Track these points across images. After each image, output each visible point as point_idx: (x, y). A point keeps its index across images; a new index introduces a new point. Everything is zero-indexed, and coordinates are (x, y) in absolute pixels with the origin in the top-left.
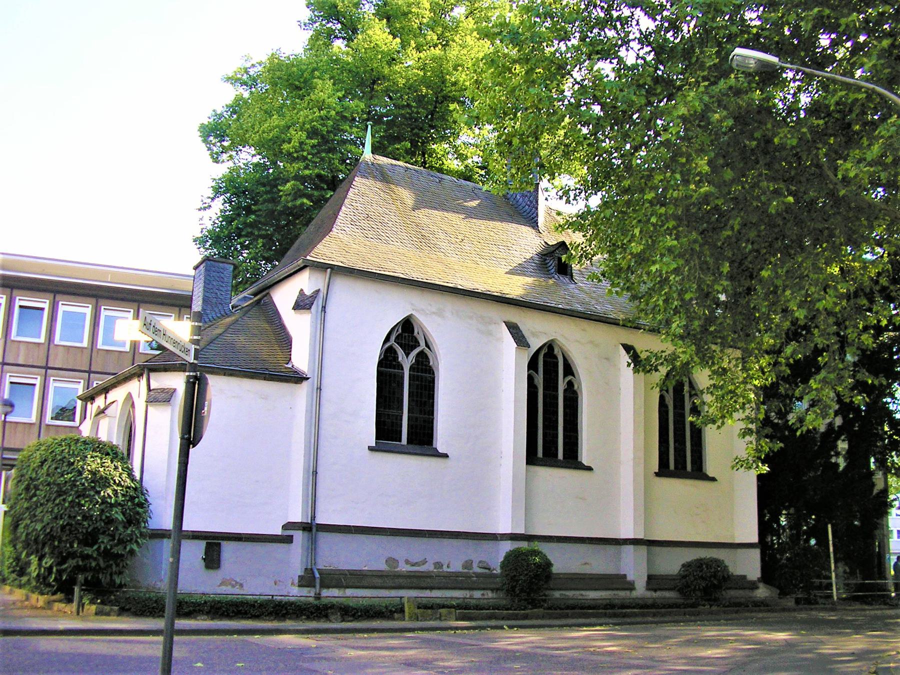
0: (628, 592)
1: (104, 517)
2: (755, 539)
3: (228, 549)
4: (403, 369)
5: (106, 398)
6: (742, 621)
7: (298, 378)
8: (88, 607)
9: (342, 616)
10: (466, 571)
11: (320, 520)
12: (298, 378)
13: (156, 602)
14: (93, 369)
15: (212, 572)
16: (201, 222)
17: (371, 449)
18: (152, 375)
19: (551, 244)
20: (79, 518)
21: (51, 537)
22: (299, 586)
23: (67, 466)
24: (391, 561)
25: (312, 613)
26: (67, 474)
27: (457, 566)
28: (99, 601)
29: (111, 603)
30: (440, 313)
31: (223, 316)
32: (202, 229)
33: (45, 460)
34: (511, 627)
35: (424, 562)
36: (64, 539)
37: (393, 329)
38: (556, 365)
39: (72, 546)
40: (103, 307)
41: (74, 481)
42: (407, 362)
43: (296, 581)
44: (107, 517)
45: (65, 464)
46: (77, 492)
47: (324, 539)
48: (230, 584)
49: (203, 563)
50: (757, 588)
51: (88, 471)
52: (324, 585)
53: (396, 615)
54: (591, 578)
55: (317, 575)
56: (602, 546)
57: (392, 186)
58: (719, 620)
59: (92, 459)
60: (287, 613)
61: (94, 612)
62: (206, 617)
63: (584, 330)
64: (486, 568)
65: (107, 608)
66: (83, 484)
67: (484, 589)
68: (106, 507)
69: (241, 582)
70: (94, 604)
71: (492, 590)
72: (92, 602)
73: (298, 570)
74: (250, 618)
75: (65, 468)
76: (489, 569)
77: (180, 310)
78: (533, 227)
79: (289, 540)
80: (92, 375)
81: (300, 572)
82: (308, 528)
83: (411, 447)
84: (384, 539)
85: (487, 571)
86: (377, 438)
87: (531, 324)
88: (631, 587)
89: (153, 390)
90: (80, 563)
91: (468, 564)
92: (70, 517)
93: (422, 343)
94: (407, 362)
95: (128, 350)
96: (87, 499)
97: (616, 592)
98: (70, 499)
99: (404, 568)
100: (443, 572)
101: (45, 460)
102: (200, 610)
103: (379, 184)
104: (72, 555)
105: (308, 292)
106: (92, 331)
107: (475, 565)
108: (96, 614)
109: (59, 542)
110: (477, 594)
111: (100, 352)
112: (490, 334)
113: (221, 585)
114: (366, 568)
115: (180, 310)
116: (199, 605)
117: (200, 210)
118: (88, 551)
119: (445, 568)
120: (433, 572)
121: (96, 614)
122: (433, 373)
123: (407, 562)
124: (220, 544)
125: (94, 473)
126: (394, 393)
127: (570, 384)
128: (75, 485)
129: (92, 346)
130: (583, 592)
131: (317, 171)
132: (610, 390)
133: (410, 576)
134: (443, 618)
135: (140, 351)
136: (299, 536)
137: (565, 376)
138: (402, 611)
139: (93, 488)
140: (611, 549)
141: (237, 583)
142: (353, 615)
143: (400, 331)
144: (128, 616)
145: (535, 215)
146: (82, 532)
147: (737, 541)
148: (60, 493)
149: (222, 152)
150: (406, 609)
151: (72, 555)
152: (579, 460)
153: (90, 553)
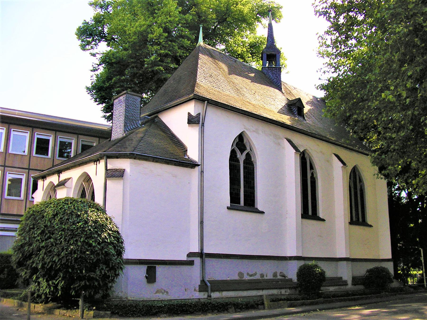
0: (344, 287)
1: (104, 252)
2: (390, 256)
3: (160, 270)
4: (239, 162)
5: (59, 177)
6: (405, 300)
7: (192, 165)
8: (87, 312)
9: (235, 309)
10: (274, 278)
11: (206, 251)
12: (192, 165)
13: (135, 307)
14: (6, 165)
15: (151, 285)
16: (91, 78)
17: (228, 208)
18: (108, 160)
19: (291, 99)
20: (88, 253)
21: (66, 266)
22: (199, 291)
23: (75, 217)
24: (241, 274)
25: (220, 308)
26: (78, 223)
27: (270, 276)
28: (94, 308)
29: (105, 309)
30: (256, 131)
31: (137, 128)
32: (92, 82)
33: (57, 214)
34: (321, 310)
35: (255, 274)
36: (76, 267)
37: (235, 139)
38: (306, 163)
39: (81, 272)
40: (12, 130)
41: (83, 227)
42: (242, 157)
43: (197, 289)
44: (106, 252)
45: (74, 216)
46: (86, 235)
47: (209, 262)
48: (161, 292)
49: (145, 280)
50: (393, 282)
51: (92, 221)
52: (213, 291)
53: (260, 306)
54: (331, 280)
55: (209, 284)
56: (330, 262)
57: (217, 61)
58: (396, 299)
59: (91, 213)
60: (209, 309)
61: (92, 316)
62: (165, 315)
63: (318, 145)
64: (283, 276)
65: (102, 313)
66: (90, 230)
67: (286, 288)
68: (105, 245)
69: (167, 290)
70: (91, 310)
71: (290, 288)
72: (90, 309)
73: (198, 282)
74: (189, 314)
75: (75, 219)
76: (285, 277)
77: (56, 133)
78: (279, 90)
79: (191, 263)
80: (6, 168)
81: (199, 283)
82: (201, 255)
83: (247, 208)
84: (235, 261)
85: (284, 278)
86: (231, 203)
87: (298, 139)
88: (345, 283)
89: (109, 170)
90: (88, 283)
91: (241, 274)
92: (81, 252)
93: (248, 148)
94: (242, 157)
95: (27, 154)
96: (93, 240)
97: (340, 287)
98: (82, 240)
99: (246, 278)
100: (265, 279)
101: (57, 214)
102: (162, 311)
103: (210, 59)
104: (81, 278)
105: (193, 114)
106: (6, 143)
107: (278, 275)
108: (94, 317)
109: (73, 270)
110: (283, 291)
111: (10, 155)
112: (279, 144)
113: (156, 293)
114: (229, 279)
115: (56, 133)
116: (161, 307)
117: (92, 71)
118: (92, 275)
119: (265, 278)
120: (260, 279)
121: (94, 317)
122: (253, 166)
123: (248, 274)
124: (155, 267)
125: (96, 222)
126: (236, 176)
127: (312, 174)
128: (84, 230)
129: (6, 151)
130: (328, 288)
131: (166, 51)
132: (330, 178)
133: (250, 282)
134: (282, 306)
135: (34, 155)
136: (197, 261)
137: (310, 170)
138: (263, 304)
139: (97, 232)
140: (334, 263)
141: (165, 291)
142: (240, 308)
143: (238, 140)
144: (116, 317)
145: (279, 84)
146: (90, 262)
147: (381, 258)
148: (73, 235)
149: (87, 44)
150: (266, 303)
151: (81, 278)
152: (318, 215)
153: (95, 276)
